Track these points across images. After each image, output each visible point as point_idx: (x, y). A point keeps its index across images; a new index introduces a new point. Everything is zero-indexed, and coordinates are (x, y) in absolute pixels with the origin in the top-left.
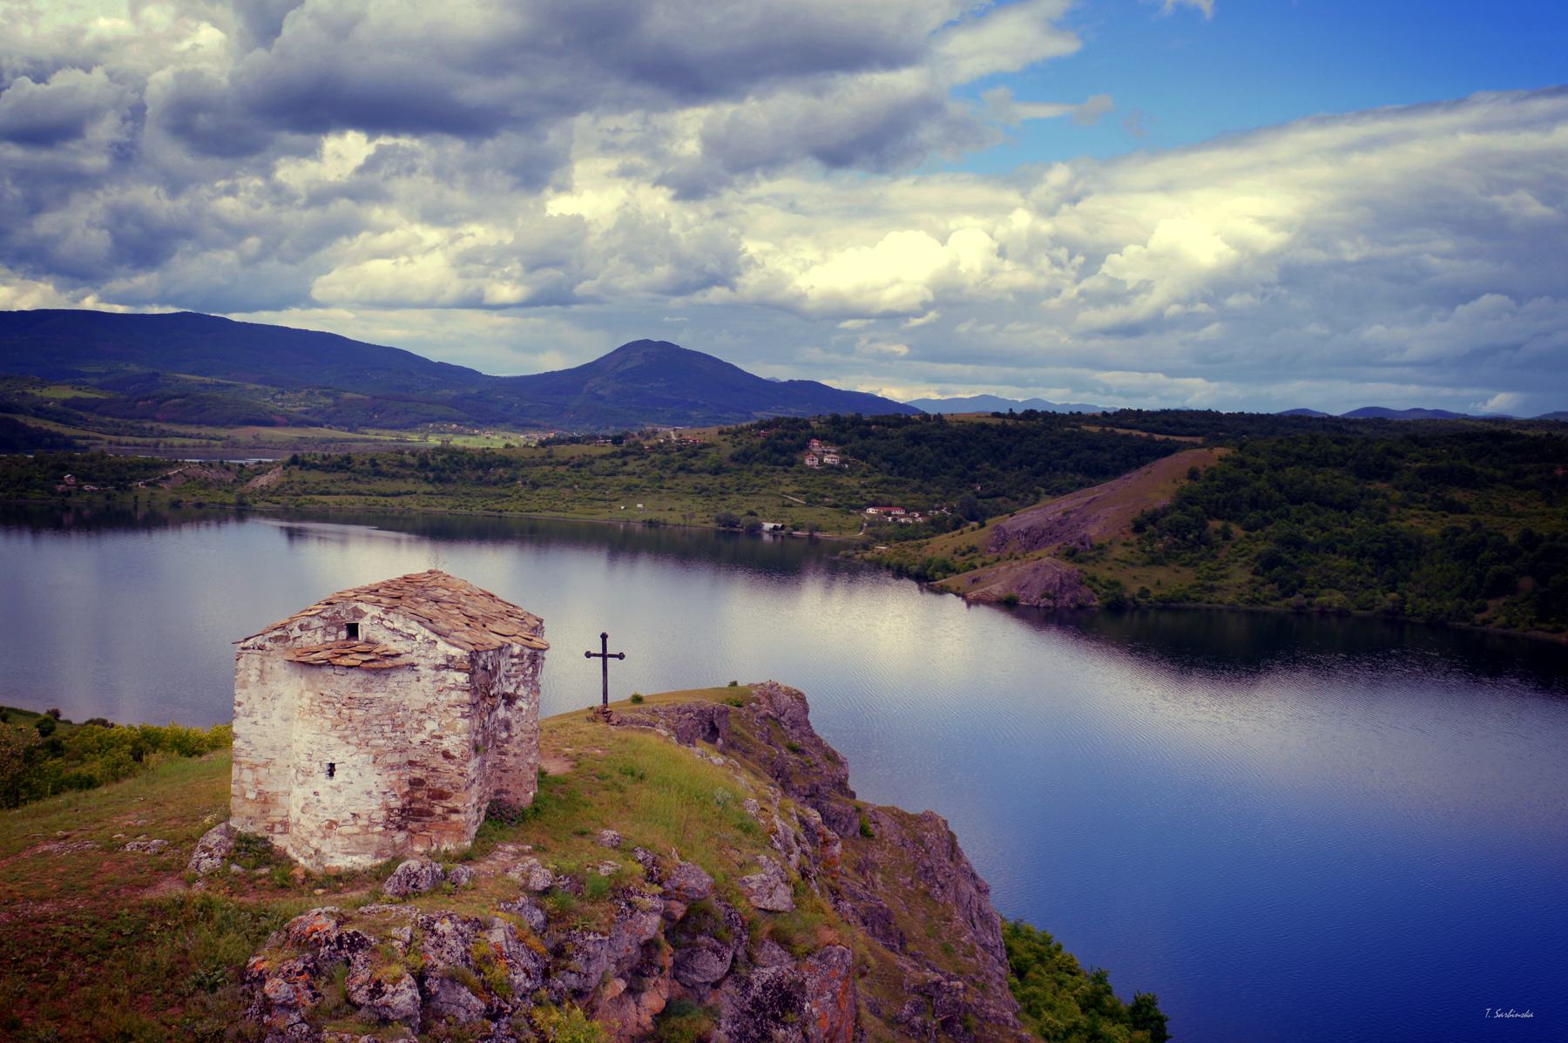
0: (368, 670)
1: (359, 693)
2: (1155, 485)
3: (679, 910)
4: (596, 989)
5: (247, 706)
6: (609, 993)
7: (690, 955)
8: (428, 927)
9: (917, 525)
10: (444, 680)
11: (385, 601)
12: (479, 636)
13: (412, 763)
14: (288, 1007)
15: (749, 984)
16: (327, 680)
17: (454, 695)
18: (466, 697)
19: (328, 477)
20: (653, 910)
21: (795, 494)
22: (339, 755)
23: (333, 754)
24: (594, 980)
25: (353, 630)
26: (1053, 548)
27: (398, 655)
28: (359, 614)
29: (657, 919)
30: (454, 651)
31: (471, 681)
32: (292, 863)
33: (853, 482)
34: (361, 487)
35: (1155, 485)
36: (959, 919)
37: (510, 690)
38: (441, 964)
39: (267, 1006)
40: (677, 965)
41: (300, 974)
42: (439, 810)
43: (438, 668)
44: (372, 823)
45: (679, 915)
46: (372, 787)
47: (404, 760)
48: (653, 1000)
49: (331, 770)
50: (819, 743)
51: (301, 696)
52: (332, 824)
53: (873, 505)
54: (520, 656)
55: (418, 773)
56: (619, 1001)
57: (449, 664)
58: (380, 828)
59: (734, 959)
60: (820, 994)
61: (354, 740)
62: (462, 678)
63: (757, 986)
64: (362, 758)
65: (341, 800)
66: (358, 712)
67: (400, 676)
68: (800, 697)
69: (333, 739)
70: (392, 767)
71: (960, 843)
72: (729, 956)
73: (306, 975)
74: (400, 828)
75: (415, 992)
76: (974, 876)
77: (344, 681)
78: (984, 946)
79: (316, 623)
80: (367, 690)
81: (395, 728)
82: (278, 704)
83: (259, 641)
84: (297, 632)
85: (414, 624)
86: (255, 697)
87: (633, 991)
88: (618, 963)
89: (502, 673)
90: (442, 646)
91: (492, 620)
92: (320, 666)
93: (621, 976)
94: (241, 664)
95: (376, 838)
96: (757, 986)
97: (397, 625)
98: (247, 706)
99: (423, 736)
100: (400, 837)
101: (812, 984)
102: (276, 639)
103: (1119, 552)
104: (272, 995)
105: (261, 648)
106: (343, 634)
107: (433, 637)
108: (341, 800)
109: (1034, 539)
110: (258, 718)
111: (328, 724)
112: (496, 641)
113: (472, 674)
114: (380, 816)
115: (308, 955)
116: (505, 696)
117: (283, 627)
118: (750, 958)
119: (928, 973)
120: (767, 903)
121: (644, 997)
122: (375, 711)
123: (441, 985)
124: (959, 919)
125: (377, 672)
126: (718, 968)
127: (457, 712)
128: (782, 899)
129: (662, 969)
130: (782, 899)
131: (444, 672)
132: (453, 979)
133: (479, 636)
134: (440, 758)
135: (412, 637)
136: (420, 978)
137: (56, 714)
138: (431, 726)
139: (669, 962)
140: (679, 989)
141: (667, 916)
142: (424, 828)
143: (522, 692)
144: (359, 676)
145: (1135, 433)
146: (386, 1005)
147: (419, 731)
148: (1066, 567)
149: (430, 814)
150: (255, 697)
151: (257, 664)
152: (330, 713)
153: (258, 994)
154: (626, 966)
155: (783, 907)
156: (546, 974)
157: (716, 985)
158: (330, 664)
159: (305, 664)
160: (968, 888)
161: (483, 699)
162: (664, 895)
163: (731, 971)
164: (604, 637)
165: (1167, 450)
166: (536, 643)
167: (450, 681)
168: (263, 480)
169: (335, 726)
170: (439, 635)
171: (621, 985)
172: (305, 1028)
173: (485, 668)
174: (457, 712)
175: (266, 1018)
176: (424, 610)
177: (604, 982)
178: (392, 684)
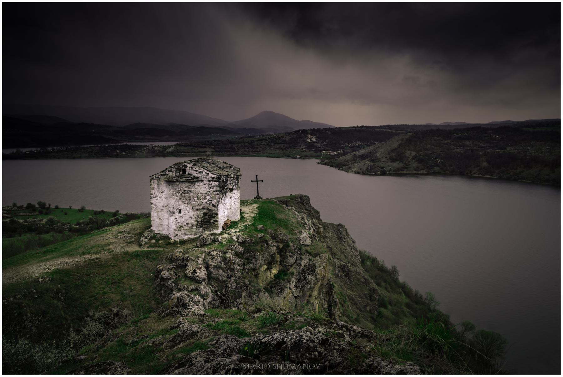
0: (189, 182)
1: (187, 189)
2: (394, 143)
3: (281, 246)
4: (259, 269)
5: (154, 195)
6: (262, 269)
7: (285, 258)
8: (209, 254)
9: (335, 155)
10: (211, 184)
11: (193, 163)
12: (221, 172)
13: (204, 209)
14: (168, 279)
15: (301, 265)
16: (178, 186)
17: (215, 189)
18: (218, 189)
19: (186, 148)
20: (274, 246)
21: (305, 148)
22: (182, 207)
23: (180, 207)
24: (258, 266)
25: (184, 171)
26: (368, 159)
27: (198, 178)
28: (186, 166)
29: (275, 248)
30: (213, 176)
31: (219, 184)
32: (170, 239)
33: (319, 145)
34: (195, 151)
35: (394, 143)
36: (348, 249)
37: (231, 187)
38: (213, 264)
39: (163, 279)
40: (281, 261)
41: (172, 269)
42: (212, 221)
43: (210, 181)
44: (193, 226)
45: (281, 247)
46: (192, 216)
47: (201, 208)
48: (275, 271)
49: (180, 211)
50: (313, 208)
51: (170, 191)
52: (181, 227)
53: (324, 150)
54: (233, 178)
55: (205, 211)
56: (265, 271)
57: (213, 179)
58: (195, 227)
59: (296, 259)
60: (320, 267)
61: (186, 202)
62: (216, 183)
63: (303, 266)
64: (189, 208)
65: (183, 220)
66: (187, 194)
67: (198, 184)
68: (308, 197)
69: (180, 203)
70: (198, 210)
71: (348, 231)
72: (295, 258)
73: (174, 270)
74: (201, 227)
75: (206, 272)
76: (352, 239)
77: (182, 186)
78: (355, 256)
79: (173, 170)
80: (189, 188)
81: (198, 199)
82: (164, 194)
83: (157, 176)
84: (168, 173)
85: (202, 169)
86: (157, 192)
87: (269, 268)
88: (264, 261)
89: (229, 182)
90: (210, 175)
91: (225, 168)
92: (175, 182)
93: (266, 264)
94: (152, 183)
95: (194, 230)
96: (303, 266)
97: (197, 169)
98: (154, 195)
99: (206, 201)
100: (201, 229)
101: (318, 264)
102: (162, 175)
103: (384, 159)
104: (163, 276)
105: (158, 178)
106: (181, 173)
107: (208, 172)
108: (183, 220)
109: (363, 157)
110: (158, 198)
111: (178, 198)
112: (226, 173)
113: (219, 182)
114: (195, 224)
115: (174, 264)
116: (230, 189)
117: (163, 171)
118: (301, 258)
119: (342, 263)
120: (305, 243)
121: (272, 270)
122: (191, 194)
123: (214, 270)
124: (348, 249)
125: (192, 183)
126: (292, 261)
127: (216, 193)
128: (309, 241)
129: (277, 262)
130: (309, 241)
131: (211, 182)
132: (217, 267)
133: (221, 172)
134: (211, 206)
135: (201, 172)
136: (207, 267)
137: (118, 211)
138: (208, 197)
139: (279, 260)
140: (281, 267)
141: (278, 247)
142: (208, 227)
143: (234, 188)
144: (186, 184)
145: (388, 130)
146: (197, 276)
147: (205, 199)
148: (371, 163)
149: (210, 222)
150: (157, 192)
151: (156, 182)
152: (178, 195)
153: (160, 276)
154: (267, 262)
155: (309, 244)
156: (244, 265)
157: (292, 266)
158: (178, 181)
159: (170, 182)
160: (350, 242)
161: (223, 189)
162: (277, 242)
163: (296, 262)
164: (257, 176)
165: (397, 134)
166: (238, 174)
167: (213, 184)
168: (170, 150)
169: (180, 199)
170: (210, 171)
171: (265, 267)
172: (174, 284)
173: (223, 180)
174: (216, 193)
175: (162, 283)
176: (205, 165)
177: (261, 266)
178: (196, 186)
